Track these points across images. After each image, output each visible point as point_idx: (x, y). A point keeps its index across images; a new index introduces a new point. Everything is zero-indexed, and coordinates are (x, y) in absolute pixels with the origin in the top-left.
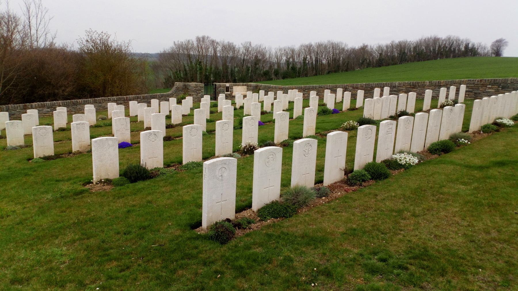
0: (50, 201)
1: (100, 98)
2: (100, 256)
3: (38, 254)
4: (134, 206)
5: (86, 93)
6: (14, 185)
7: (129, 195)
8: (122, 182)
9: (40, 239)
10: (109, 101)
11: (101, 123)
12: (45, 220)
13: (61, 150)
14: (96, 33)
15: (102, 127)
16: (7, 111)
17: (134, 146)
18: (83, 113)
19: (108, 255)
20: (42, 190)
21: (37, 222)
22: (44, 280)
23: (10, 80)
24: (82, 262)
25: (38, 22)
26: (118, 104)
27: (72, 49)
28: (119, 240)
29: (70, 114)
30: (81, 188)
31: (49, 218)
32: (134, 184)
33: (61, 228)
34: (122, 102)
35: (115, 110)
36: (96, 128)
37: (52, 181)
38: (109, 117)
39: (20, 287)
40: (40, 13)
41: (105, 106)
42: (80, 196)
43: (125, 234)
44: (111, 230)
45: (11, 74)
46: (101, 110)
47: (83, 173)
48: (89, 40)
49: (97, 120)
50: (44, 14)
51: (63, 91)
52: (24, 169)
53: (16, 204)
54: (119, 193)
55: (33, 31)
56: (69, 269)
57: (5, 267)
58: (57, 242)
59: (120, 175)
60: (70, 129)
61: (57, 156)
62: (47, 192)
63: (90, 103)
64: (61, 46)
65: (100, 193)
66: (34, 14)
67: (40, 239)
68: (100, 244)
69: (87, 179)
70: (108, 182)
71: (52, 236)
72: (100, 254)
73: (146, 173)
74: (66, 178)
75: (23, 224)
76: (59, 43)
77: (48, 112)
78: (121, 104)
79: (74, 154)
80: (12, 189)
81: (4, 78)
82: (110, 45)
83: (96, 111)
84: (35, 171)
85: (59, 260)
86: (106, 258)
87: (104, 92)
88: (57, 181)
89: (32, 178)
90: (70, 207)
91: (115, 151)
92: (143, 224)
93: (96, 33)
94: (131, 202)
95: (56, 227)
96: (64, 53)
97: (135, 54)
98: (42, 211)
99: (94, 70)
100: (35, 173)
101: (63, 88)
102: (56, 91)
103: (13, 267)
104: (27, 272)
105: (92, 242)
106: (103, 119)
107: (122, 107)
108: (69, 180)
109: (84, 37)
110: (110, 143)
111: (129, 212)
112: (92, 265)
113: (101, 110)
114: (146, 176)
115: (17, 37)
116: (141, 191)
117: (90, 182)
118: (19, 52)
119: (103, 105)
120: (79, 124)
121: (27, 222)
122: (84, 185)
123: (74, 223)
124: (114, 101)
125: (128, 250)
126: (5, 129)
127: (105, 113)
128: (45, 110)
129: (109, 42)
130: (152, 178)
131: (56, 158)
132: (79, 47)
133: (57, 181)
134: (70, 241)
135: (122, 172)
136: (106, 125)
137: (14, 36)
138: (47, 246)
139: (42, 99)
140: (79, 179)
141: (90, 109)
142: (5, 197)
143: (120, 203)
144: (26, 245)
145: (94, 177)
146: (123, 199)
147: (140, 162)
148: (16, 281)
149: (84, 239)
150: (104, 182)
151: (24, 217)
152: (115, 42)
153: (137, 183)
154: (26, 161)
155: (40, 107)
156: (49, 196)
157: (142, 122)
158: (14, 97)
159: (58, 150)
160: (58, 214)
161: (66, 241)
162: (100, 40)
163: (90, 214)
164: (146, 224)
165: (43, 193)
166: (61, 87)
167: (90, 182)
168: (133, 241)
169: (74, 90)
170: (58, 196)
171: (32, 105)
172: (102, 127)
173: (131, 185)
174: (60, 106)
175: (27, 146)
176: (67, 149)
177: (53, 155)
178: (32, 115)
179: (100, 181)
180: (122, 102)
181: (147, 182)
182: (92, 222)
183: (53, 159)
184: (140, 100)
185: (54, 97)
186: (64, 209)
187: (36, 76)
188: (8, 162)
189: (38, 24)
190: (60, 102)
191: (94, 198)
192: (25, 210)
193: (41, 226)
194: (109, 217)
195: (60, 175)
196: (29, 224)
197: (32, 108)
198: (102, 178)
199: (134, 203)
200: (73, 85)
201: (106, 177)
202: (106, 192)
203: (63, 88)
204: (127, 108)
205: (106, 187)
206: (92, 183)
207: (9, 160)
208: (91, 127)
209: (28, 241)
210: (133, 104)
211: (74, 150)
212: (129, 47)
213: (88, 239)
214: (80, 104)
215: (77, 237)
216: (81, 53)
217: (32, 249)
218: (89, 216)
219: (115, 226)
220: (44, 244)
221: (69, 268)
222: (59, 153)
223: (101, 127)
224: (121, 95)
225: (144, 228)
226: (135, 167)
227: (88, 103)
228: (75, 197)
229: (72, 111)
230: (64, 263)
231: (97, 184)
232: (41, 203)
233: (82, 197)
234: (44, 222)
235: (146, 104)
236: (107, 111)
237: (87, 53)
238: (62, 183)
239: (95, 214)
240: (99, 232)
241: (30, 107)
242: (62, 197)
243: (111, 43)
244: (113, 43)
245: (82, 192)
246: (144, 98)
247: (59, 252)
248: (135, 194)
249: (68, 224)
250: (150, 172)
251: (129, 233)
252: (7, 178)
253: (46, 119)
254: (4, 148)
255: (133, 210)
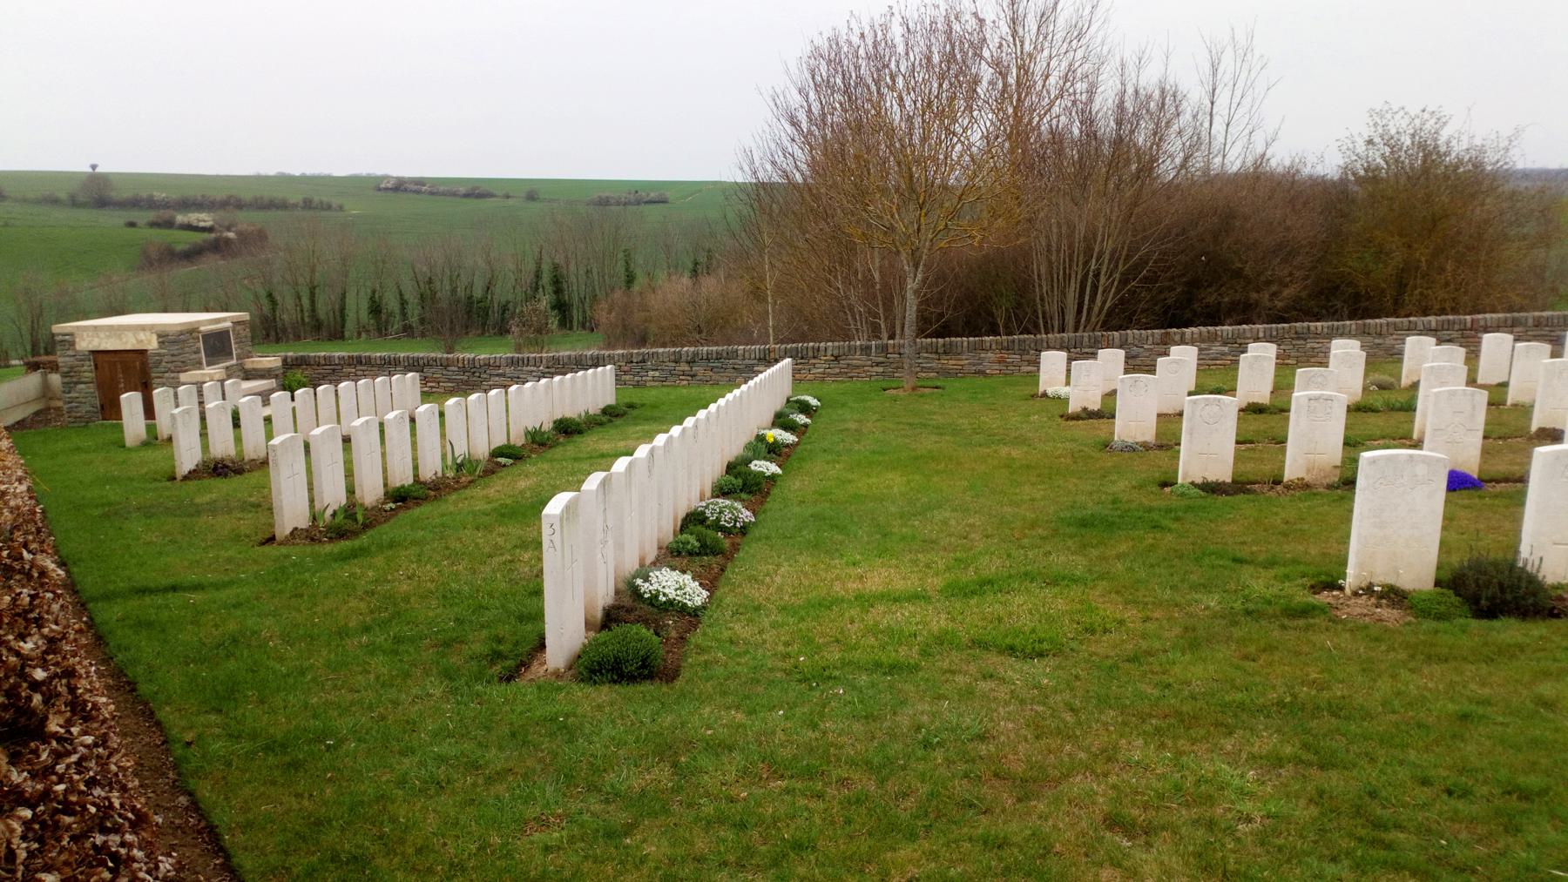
0: (1214, 616)
1: (1383, 321)
2: (1361, 840)
3: (1176, 763)
4: (1486, 702)
5: (1339, 305)
6: (1123, 548)
7: (1465, 659)
8: (1442, 608)
9: (1183, 721)
10: (1412, 329)
11: (1378, 400)
12: (1198, 670)
13: (1250, 469)
14: (1402, 113)
15: (1384, 414)
16: (1121, 347)
17: (1489, 487)
18: (1325, 364)
19: (1388, 846)
20: (1194, 578)
21: (1177, 669)
22: (1191, 848)
23: (1143, 262)
24: (1301, 836)
25: (1236, 100)
26: (1440, 342)
27: (1320, 170)
28: (1424, 806)
29: (1285, 368)
30: (1304, 597)
31: (1211, 667)
32: (1485, 623)
33: (1241, 706)
34: (1455, 335)
35: (1427, 359)
36: (1359, 414)
37: (1222, 558)
38: (1405, 382)
39: (1126, 843)
40: (1244, 75)
41: (1393, 347)
42: (1301, 622)
43: (1450, 793)
44: (1401, 763)
45: (1143, 251)
46: (1383, 357)
47: (1313, 551)
48: (1377, 140)
49: (1365, 389)
50: (1253, 74)
51: (1274, 294)
52: (1150, 510)
53: (1127, 603)
54: (1433, 645)
55: (1219, 127)
56: (1262, 844)
57: (1093, 772)
58: (1228, 744)
59: (1438, 583)
60: (1113, 417)
61: (1239, 486)
62: (1206, 587)
63: (1350, 335)
64: (1287, 163)
65: (1366, 627)
66: (1227, 78)
67: (1183, 721)
68: (1360, 798)
69: (1327, 574)
70: (1394, 596)
71: (1217, 725)
72: (1362, 832)
73: (1534, 595)
74: (1262, 557)
75: (1141, 664)
76: (1280, 158)
77: (1223, 354)
78: (1450, 341)
79: (1288, 487)
80: (1118, 557)
81: (1128, 258)
82: (1443, 149)
83: (1367, 363)
84: (1177, 519)
85: (1233, 802)
86: (1383, 853)
87: (1396, 302)
88: (1235, 560)
89: (1169, 537)
90: (1269, 649)
91: (1436, 495)
92: (1522, 780)
93: (1402, 113)
94: (1473, 686)
95: (1227, 698)
96: (1293, 182)
97: (1526, 175)
98: (1193, 642)
99: (1377, 233)
100: (1174, 526)
101: (1274, 288)
102: (1254, 295)
103: (1113, 779)
104: (1146, 807)
105: (1334, 780)
106: (1382, 387)
107: (1459, 352)
108: (1270, 564)
109: (1362, 129)
110: (1421, 470)
111: (1465, 717)
112: (1334, 860)
113: (1383, 357)
114: (1534, 605)
115: (1174, 146)
116: (1513, 656)
117: (1333, 585)
118: (1171, 189)
119: (1389, 341)
120: (1317, 399)
121: (1151, 659)
122: (1316, 589)
123: (1281, 704)
124: (1428, 331)
125: (1460, 854)
126: (1114, 392)
127: (1391, 367)
128: (1217, 348)
129: (1442, 140)
130: (1557, 616)
131: (1235, 493)
132: (1341, 163)
133: (1235, 560)
134: (1267, 757)
135: (1446, 575)
136: (1392, 409)
137: (1165, 146)
138: (1201, 748)
139: (1213, 317)
140: (1302, 568)
141: (1347, 356)
142: (1101, 577)
143: (1426, 681)
144: (1147, 728)
145: (1350, 571)
146: (1444, 666)
147: (1517, 552)
148: (1117, 824)
149: (1310, 764)
150: (1381, 596)
151: (1144, 645)
152: (1465, 138)
153: (1496, 624)
154: (1155, 489)
155: (1203, 341)
156: (1213, 601)
157: (1525, 410)
158: (1143, 311)
159: (1242, 468)
160: (1235, 661)
161: (1255, 749)
162: (1413, 136)
163: (1329, 688)
164: (1533, 781)
165: (1194, 587)
166: (1268, 283)
167: (1333, 585)
168: (1481, 830)
169: (1304, 294)
170: (1238, 605)
171: (1183, 334)
172: (1384, 414)
173: (1475, 624)
174: (1257, 339)
175: (1160, 447)
176: (1267, 469)
177: (1229, 480)
178: (1181, 360)
179: (1369, 590)
180: (1455, 335)
181: (1537, 630)
182: (1334, 714)
183: (1228, 494)
184: (1523, 332)
185: (1244, 312)
186: (1252, 649)
187: (1206, 254)
188: (1113, 482)
189: (1234, 106)
190: (1260, 327)
191: (1345, 640)
192: (1148, 625)
193: (1189, 684)
194: (1394, 718)
195: (1244, 543)
196: (1157, 668)
197: (1183, 342)
198: (1376, 580)
199: (1487, 691)
200: (1307, 277)
201: (1391, 581)
202: (1387, 630)
203: (1274, 288)
204: (1473, 357)
205: (1388, 614)
206: (1341, 589)
207: (1114, 477)
208: (1349, 409)
209: (1150, 716)
210: (1495, 345)
211: (1290, 474)
212: (1511, 153)
213: (1322, 767)
214: (1317, 335)
215: (1288, 750)
216: (1343, 181)
217: (1162, 746)
218: (1326, 694)
219: (1412, 755)
220: (1194, 742)
221: (1262, 839)
222: (1243, 479)
223: (1374, 410)
224: (1454, 311)
225: (1525, 795)
226: (1495, 564)
227: (1342, 335)
228: (1286, 622)
229: (1289, 357)
230: (1249, 820)
231: (1355, 594)
232: (1190, 615)
233: (1307, 628)
234: (1198, 673)
235: (1547, 347)
236: (1401, 361)
237: (1360, 181)
238: (1251, 569)
239: (1346, 692)
240: (1358, 755)
241: (1177, 338)
242: (1248, 613)
243: (1448, 143)
244: (1454, 143)
245: (1306, 612)
246: (1538, 324)
247: (1237, 782)
248: (1489, 660)
249: (1262, 700)
250: (1553, 594)
251: (1465, 794)
252: (1110, 525)
253: (1216, 377)
254: (1106, 445)
255: (1482, 717)
